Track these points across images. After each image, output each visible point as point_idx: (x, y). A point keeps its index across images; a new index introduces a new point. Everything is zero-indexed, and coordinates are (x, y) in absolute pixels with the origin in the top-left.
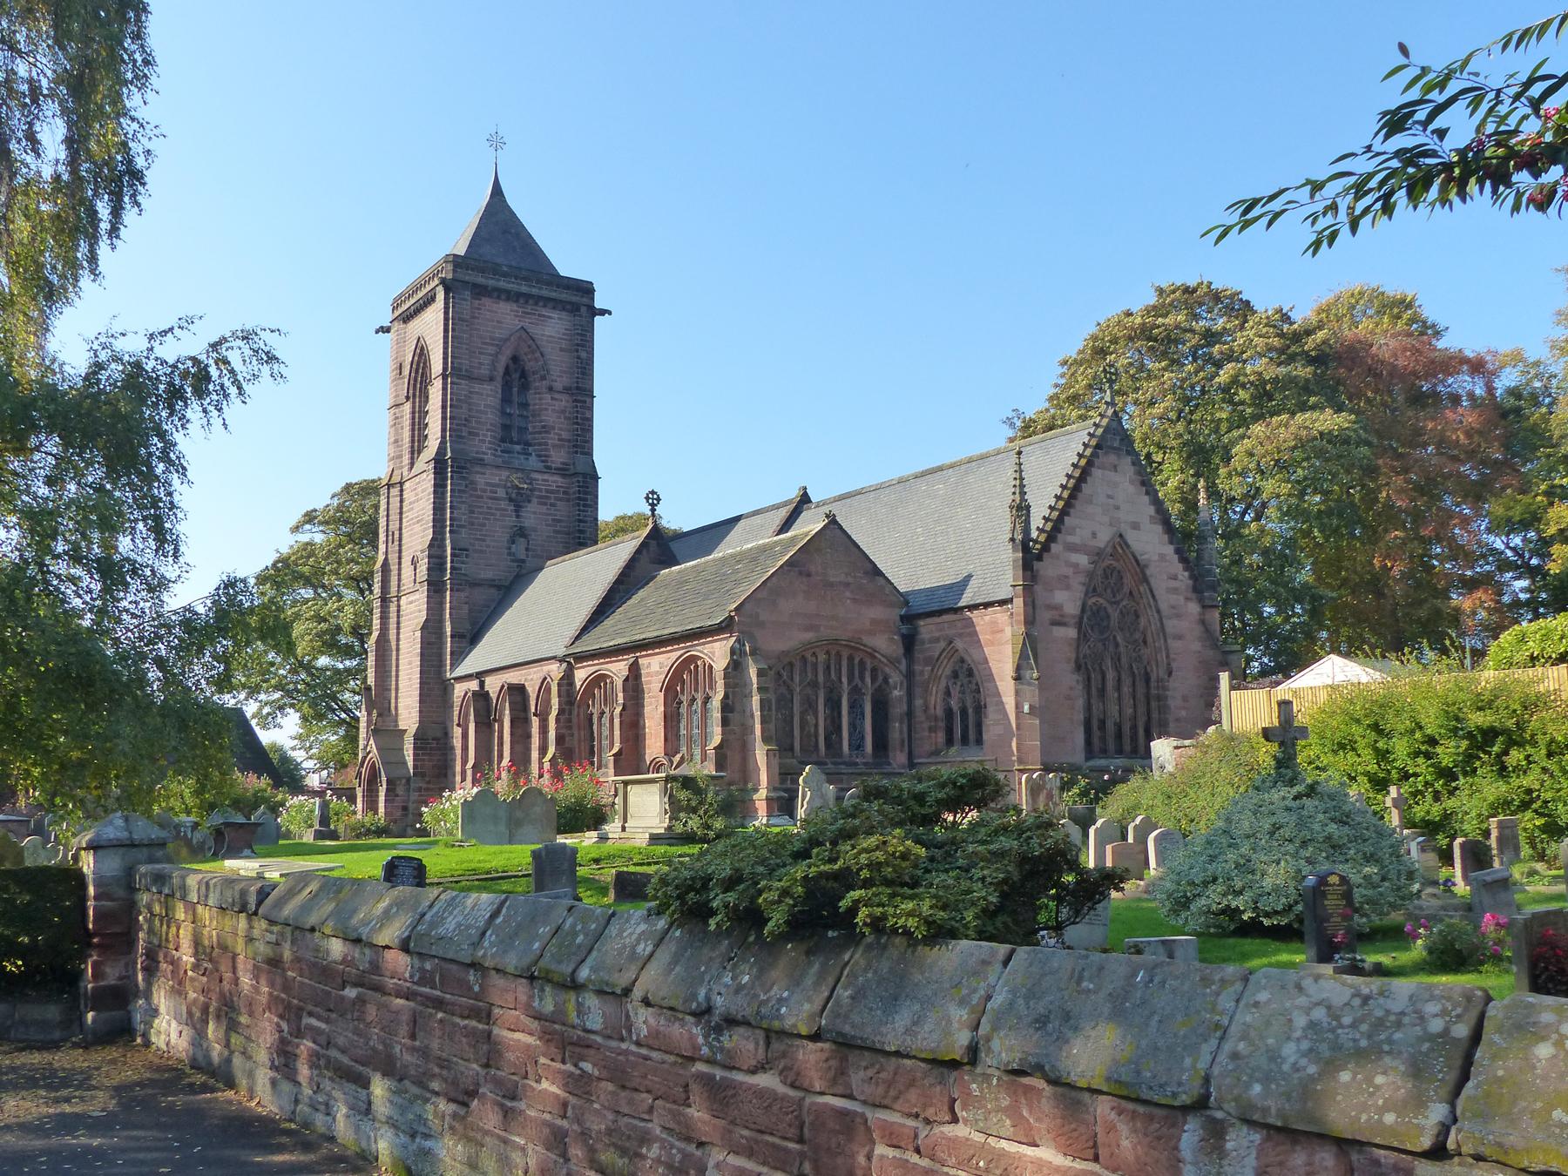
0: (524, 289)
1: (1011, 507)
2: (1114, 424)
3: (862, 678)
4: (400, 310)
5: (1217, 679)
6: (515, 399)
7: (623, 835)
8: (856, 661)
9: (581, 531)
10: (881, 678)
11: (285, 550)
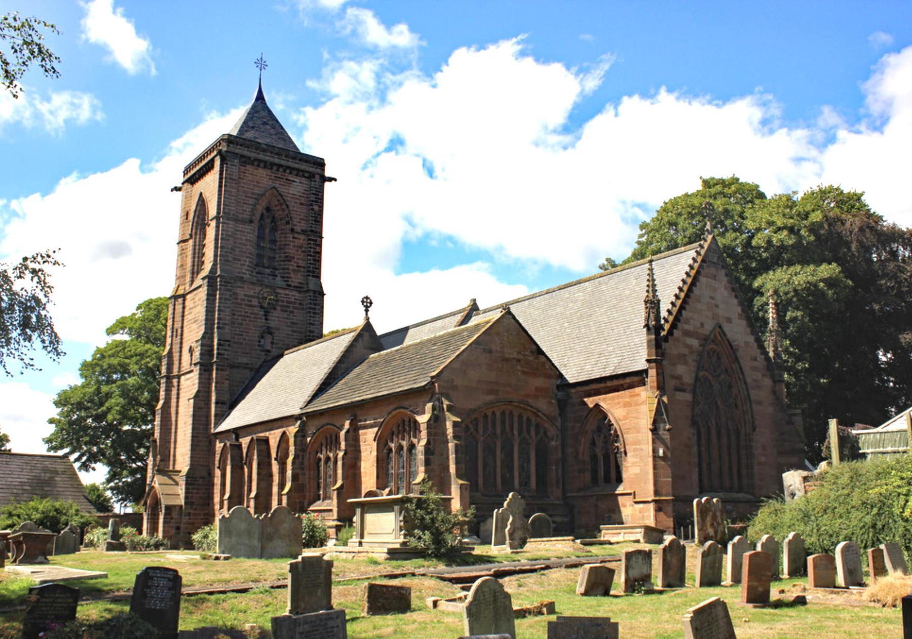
0: (276, 161)
1: (646, 302)
2: (714, 246)
3: (528, 432)
4: (189, 175)
5: (827, 424)
6: (267, 237)
7: (361, 549)
8: (525, 418)
9: (311, 332)
10: (542, 431)
11: (102, 346)
